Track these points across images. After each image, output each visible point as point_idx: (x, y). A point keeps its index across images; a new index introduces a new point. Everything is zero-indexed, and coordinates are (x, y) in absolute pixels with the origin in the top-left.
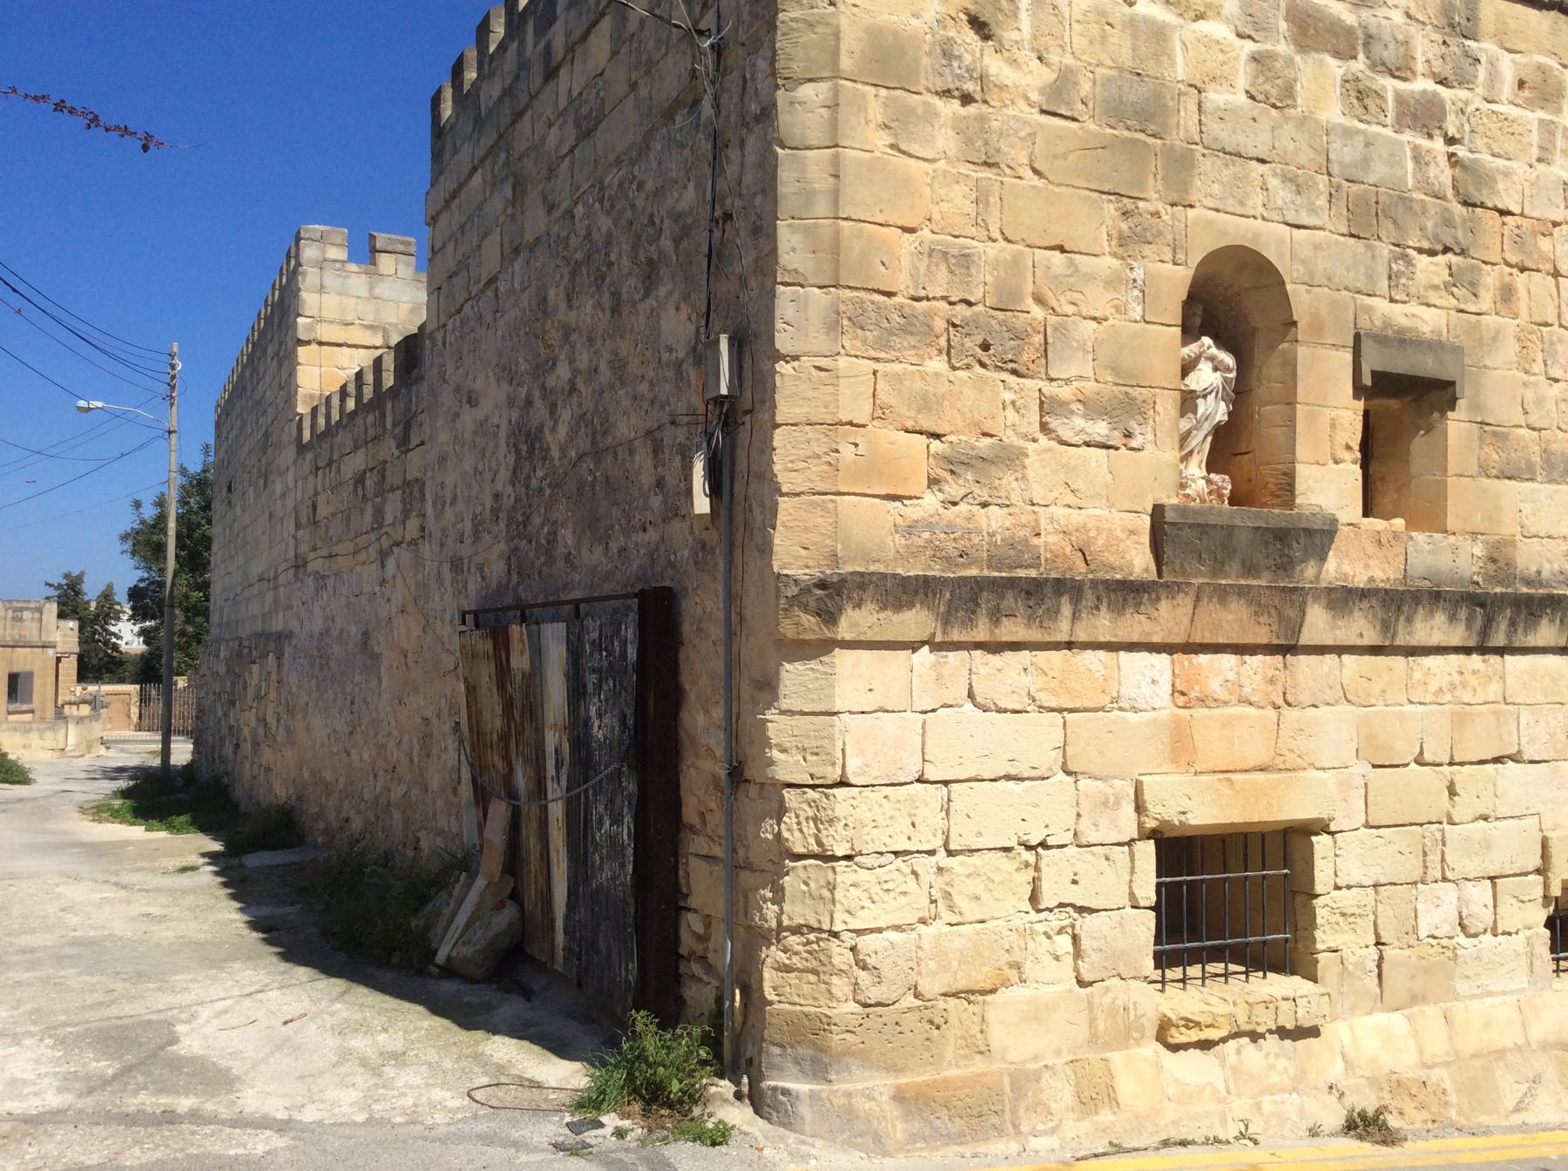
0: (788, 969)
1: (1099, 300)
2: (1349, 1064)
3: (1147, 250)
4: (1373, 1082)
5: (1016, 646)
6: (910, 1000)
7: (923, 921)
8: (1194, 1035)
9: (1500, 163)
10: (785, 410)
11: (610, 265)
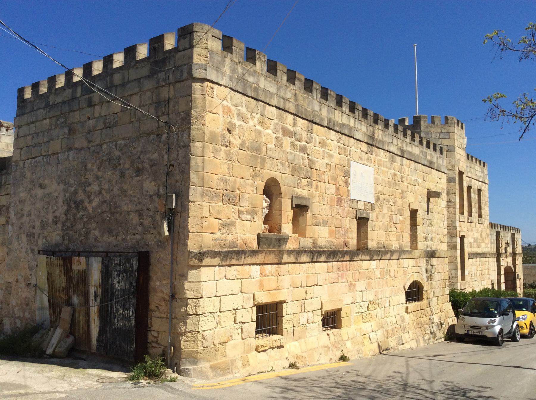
0: (187, 341)
1: (249, 189)
2: (289, 353)
3: (257, 178)
4: (293, 356)
5: (233, 265)
6: (213, 346)
7: (215, 328)
8: (263, 349)
9: (316, 159)
10: (191, 214)
11: (120, 164)
